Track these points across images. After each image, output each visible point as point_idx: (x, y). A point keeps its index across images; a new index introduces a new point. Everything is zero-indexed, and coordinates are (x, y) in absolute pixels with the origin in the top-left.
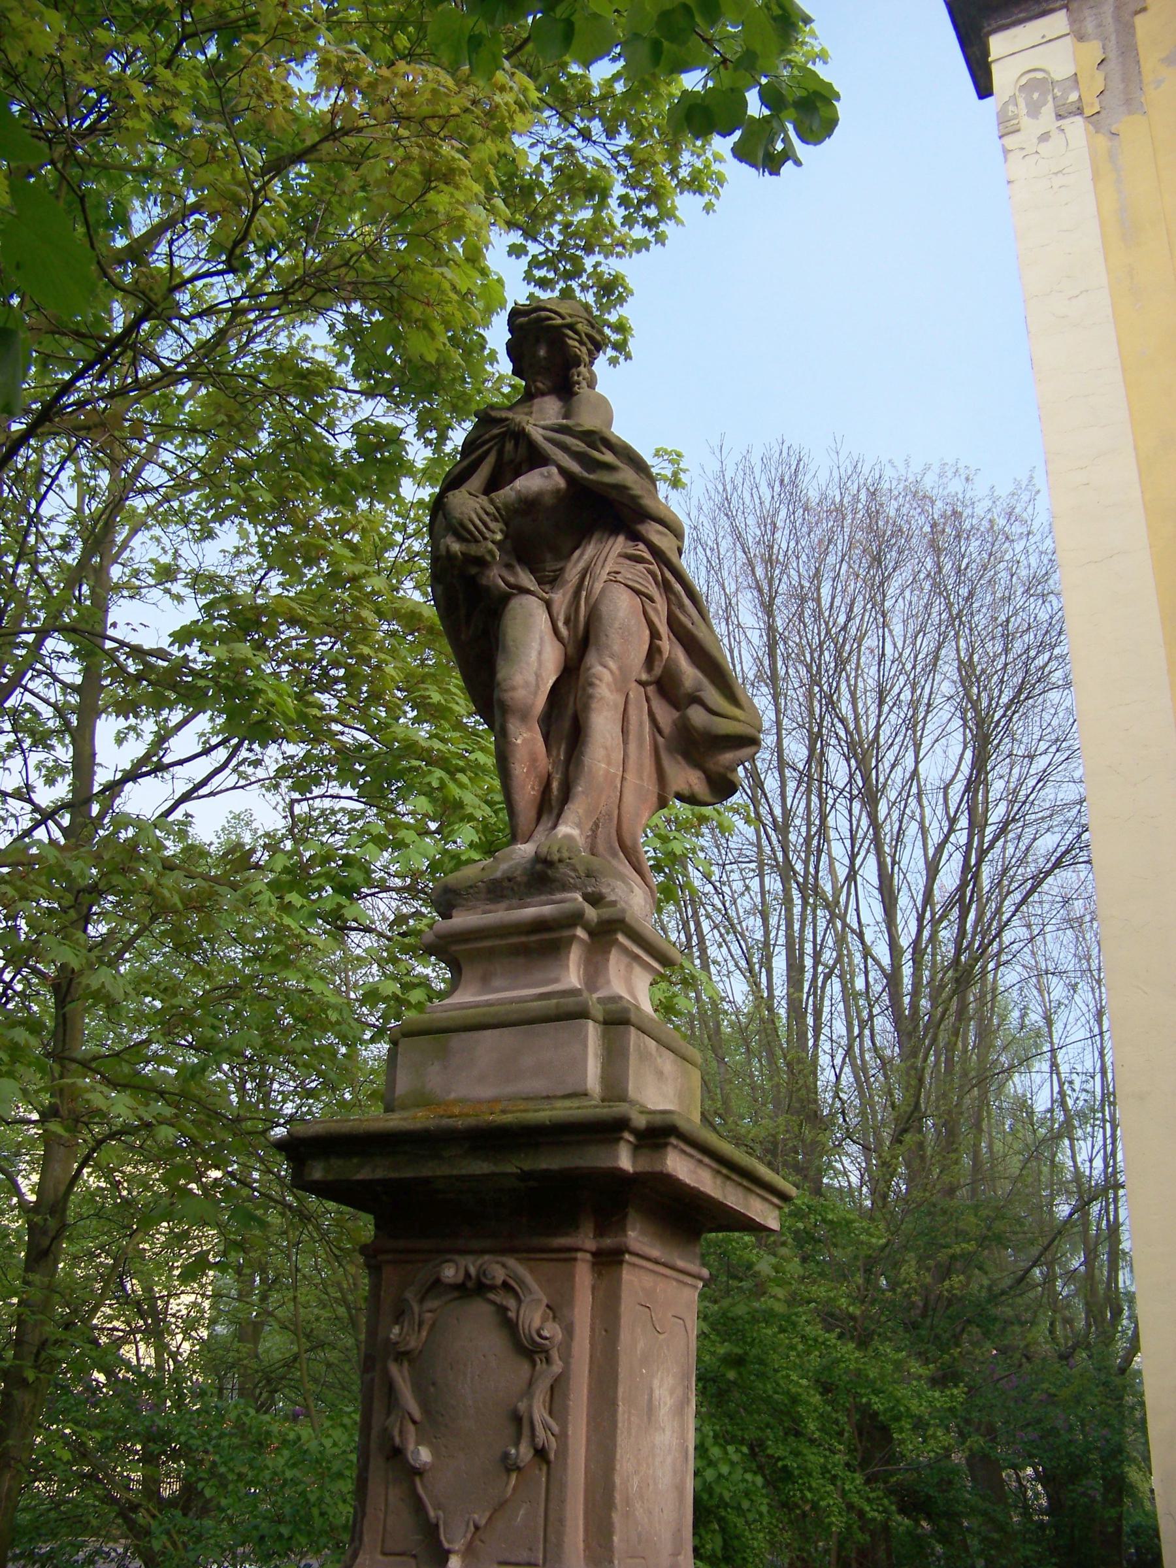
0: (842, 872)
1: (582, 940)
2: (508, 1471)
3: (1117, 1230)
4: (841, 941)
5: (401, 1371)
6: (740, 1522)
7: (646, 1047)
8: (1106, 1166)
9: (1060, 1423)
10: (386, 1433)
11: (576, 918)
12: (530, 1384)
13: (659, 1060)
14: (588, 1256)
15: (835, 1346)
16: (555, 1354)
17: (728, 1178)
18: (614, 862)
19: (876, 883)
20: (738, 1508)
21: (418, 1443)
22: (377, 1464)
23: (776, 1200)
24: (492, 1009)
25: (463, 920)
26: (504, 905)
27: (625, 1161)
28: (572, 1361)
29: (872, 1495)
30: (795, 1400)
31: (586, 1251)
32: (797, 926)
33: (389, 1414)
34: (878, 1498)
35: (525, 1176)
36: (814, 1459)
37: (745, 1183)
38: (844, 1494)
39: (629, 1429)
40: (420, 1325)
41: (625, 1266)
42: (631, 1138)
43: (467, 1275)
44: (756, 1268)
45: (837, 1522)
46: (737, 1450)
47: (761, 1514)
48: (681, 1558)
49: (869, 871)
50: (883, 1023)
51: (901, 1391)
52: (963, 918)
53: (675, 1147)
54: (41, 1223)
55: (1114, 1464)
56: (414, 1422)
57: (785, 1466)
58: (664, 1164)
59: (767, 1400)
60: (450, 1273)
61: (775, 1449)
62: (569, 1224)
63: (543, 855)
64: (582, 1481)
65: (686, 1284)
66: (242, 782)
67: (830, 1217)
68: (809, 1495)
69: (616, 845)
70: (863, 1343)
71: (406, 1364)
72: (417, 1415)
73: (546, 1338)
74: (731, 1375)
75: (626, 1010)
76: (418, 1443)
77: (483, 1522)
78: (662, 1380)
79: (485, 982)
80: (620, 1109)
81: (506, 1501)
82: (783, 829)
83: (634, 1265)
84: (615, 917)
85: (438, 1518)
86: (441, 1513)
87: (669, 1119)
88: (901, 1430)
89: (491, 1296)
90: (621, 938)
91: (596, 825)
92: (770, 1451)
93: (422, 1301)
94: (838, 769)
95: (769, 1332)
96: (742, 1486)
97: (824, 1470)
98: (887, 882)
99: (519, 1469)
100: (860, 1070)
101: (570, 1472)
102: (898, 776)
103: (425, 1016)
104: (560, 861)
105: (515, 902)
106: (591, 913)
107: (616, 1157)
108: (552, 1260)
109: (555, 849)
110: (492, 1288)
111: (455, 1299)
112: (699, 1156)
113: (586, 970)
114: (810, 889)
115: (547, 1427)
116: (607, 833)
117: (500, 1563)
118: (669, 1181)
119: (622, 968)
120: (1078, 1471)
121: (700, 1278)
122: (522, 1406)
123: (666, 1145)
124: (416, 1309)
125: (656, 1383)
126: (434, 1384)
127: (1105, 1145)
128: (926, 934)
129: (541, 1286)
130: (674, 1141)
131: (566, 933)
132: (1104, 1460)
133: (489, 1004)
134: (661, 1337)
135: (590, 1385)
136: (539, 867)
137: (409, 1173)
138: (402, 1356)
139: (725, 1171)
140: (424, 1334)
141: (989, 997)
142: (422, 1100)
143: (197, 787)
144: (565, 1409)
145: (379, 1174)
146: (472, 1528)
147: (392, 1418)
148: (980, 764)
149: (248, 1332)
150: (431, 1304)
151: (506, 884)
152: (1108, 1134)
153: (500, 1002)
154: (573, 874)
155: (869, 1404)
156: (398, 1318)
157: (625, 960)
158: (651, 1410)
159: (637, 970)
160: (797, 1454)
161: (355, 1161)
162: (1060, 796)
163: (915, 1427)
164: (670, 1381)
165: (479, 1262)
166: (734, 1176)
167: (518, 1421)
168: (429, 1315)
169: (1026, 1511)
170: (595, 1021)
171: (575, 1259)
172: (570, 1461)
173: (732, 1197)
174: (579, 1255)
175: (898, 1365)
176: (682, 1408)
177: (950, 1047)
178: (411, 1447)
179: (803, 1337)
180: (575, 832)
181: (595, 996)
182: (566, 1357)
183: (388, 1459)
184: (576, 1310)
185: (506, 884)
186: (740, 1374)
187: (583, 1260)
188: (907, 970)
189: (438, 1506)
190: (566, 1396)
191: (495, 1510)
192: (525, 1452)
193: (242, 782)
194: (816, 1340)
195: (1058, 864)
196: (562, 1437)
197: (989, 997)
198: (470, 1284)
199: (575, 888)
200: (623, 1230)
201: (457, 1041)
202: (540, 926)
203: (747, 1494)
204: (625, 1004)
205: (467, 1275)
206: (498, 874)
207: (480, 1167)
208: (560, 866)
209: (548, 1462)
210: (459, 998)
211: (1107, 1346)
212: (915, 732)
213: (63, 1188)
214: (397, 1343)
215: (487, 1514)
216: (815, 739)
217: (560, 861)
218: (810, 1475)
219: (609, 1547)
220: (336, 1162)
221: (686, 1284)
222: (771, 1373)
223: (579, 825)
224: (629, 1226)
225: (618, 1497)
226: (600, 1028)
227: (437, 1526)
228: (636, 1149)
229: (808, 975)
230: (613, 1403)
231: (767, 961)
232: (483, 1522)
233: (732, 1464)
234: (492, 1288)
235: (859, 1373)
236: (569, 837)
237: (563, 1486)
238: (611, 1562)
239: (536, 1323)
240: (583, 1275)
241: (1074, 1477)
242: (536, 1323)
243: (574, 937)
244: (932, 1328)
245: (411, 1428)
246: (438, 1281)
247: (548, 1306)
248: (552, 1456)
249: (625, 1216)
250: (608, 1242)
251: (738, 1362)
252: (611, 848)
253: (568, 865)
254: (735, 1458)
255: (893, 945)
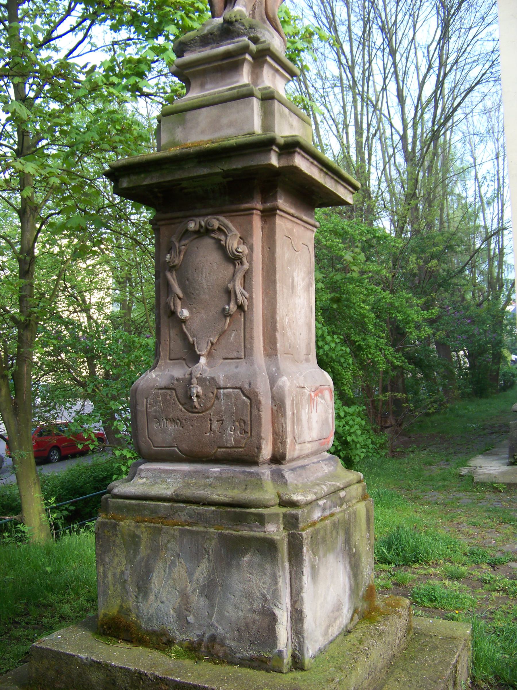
0: (379, 88)
1: (249, 61)
2: (226, 316)
3: (503, 250)
4: (379, 121)
5: (172, 276)
6: (340, 368)
7: (283, 111)
8: (498, 223)
9: (476, 332)
10: (167, 305)
11: (245, 49)
12: (234, 275)
13: (290, 119)
14: (259, 212)
15: (380, 292)
16: (245, 260)
17: (326, 174)
18: (265, 25)
19: (396, 94)
20: (339, 362)
21: (182, 308)
22: (164, 319)
23: (351, 189)
24: (206, 98)
25: (189, 57)
26: (209, 47)
27: (274, 161)
28: (253, 262)
29: (397, 356)
30: (364, 316)
31: (258, 210)
32: (359, 117)
33: (168, 297)
34: (400, 357)
35: (226, 174)
36: (372, 341)
37: (335, 177)
38: (385, 355)
39: (283, 294)
40: (179, 253)
41: (277, 217)
42: (277, 150)
43: (201, 226)
44: (345, 258)
45: (382, 367)
46: (338, 338)
47: (349, 364)
48: (310, 356)
49: (392, 87)
50: (400, 159)
51: (409, 311)
52: (436, 107)
53: (299, 153)
54: (23, 258)
55: (497, 348)
56: (180, 299)
57: (359, 345)
58: (293, 161)
59: (351, 318)
60: (192, 226)
61: (354, 337)
62: (249, 197)
63: (227, 19)
64: (261, 319)
65: (308, 229)
66: (94, 49)
67: (377, 235)
68: (370, 356)
69: (265, 17)
70: (393, 292)
71: (174, 272)
72: (181, 295)
73: (240, 252)
74: (335, 306)
75: (272, 92)
76: (182, 308)
77: (215, 341)
78: (298, 274)
79: (202, 86)
80: (270, 135)
81: (225, 331)
82: (352, 69)
83: (282, 216)
84: (265, 48)
85: (194, 341)
86: (195, 339)
87: (295, 138)
88: (410, 328)
89: (213, 235)
90: (268, 59)
91: (254, 7)
92: (353, 338)
93: (180, 241)
94: (378, 37)
95: (351, 286)
96: (341, 353)
97: (377, 346)
98: (400, 93)
99: (231, 316)
100: (390, 181)
101: (254, 315)
102: (405, 43)
103: (173, 106)
104: (236, 21)
105: (214, 45)
106: (253, 47)
107: (270, 159)
108: (241, 215)
109: (233, 15)
110: (213, 231)
111: (194, 239)
112: (312, 160)
113: (252, 77)
114: (366, 100)
115: (243, 295)
116: (260, 11)
117: (224, 359)
118: (296, 170)
119: (270, 76)
120: (483, 351)
121: (316, 227)
122: (230, 286)
123: (294, 152)
124: (177, 245)
125: (295, 274)
126: (188, 280)
127: (498, 214)
128: (419, 114)
129: (236, 228)
130: (298, 150)
131: (241, 58)
132: (493, 347)
133: (204, 96)
134: (297, 253)
135: (263, 275)
136: (225, 25)
137: (169, 178)
138: (172, 268)
139: (325, 170)
140: (182, 256)
141: (447, 146)
142: (174, 144)
143: (71, 52)
144: (251, 285)
145: (154, 181)
146: (210, 344)
147: (170, 297)
148: (445, 36)
149: (126, 307)
150: (183, 242)
151: (210, 36)
152: (500, 208)
153: (210, 94)
154: (243, 28)
155: (396, 316)
156: (169, 251)
157: (271, 72)
158: (293, 287)
159: (278, 78)
160: (365, 340)
161: (142, 176)
162: (483, 49)
163: (416, 328)
164: (302, 274)
165: (206, 219)
166: (330, 174)
167: (229, 294)
168: (183, 247)
169: (460, 368)
170: (257, 98)
171: (252, 214)
172: (254, 310)
173: (329, 184)
174: (254, 212)
175: (407, 300)
176: (309, 288)
177: (430, 168)
178: (179, 310)
179: (366, 288)
180: (244, 9)
181: (257, 88)
182: (250, 262)
183: (169, 317)
184: (254, 238)
185: (210, 36)
186: (339, 306)
187: (256, 214)
188: (410, 133)
189: (193, 336)
190: (251, 279)
191: (220, 335)
192: (233, 307)
193: (94, 49)
194: (372, 290)
195: (478, 83)
196: (250, 299)
197: (447, 146)
198: (202, 230)
199: (244, 35)
200: (276, 200)
201: (189, 115)
202: (228, 55)
203: (342, 356)
204: (271, 89)
205: (201, 226)
206: (206, 32)
207: (204, 171)
208: (236, 24)
209: (244, 311)
210: (189, 96)
211: (497, 299)
212: (414, 18)
213: (31, 243)
214: (169, 262)
215: (217, 337)
216: (367, 22)
217: (236, 21)
218: (370, 347)
219: (275, 349)
220: (133, 178)
221: (308, 229)
222: (352, 305)
223: (245, 6)
224: (278, 197)
225: (278, 325)
226: (260, 102)
227: (194, 344)
228: (280, 156)
229: (365, 132)
230: (274, 282)
231: (346, 126)
232: (215, 341)
233: (336, 343)
234: (213, 231)
235: (391, 304)
236: (240, 11)
237: (251, 321)
238: (276, 355)
239: (235, 246)
240: (257, 222)
241: (481, 354)
242: (235, 246)
243: (245, 59)
244: (423, 288)
245: (179, 302)
246: (187, 231)
247: (240, 238)
248: (246, 308)
249: (276, 192)
250: (268, 205)
251: (337, 300)
252: (262, 19)
253: (240, 23)
254: (337, 341)
255: (403, 119)
